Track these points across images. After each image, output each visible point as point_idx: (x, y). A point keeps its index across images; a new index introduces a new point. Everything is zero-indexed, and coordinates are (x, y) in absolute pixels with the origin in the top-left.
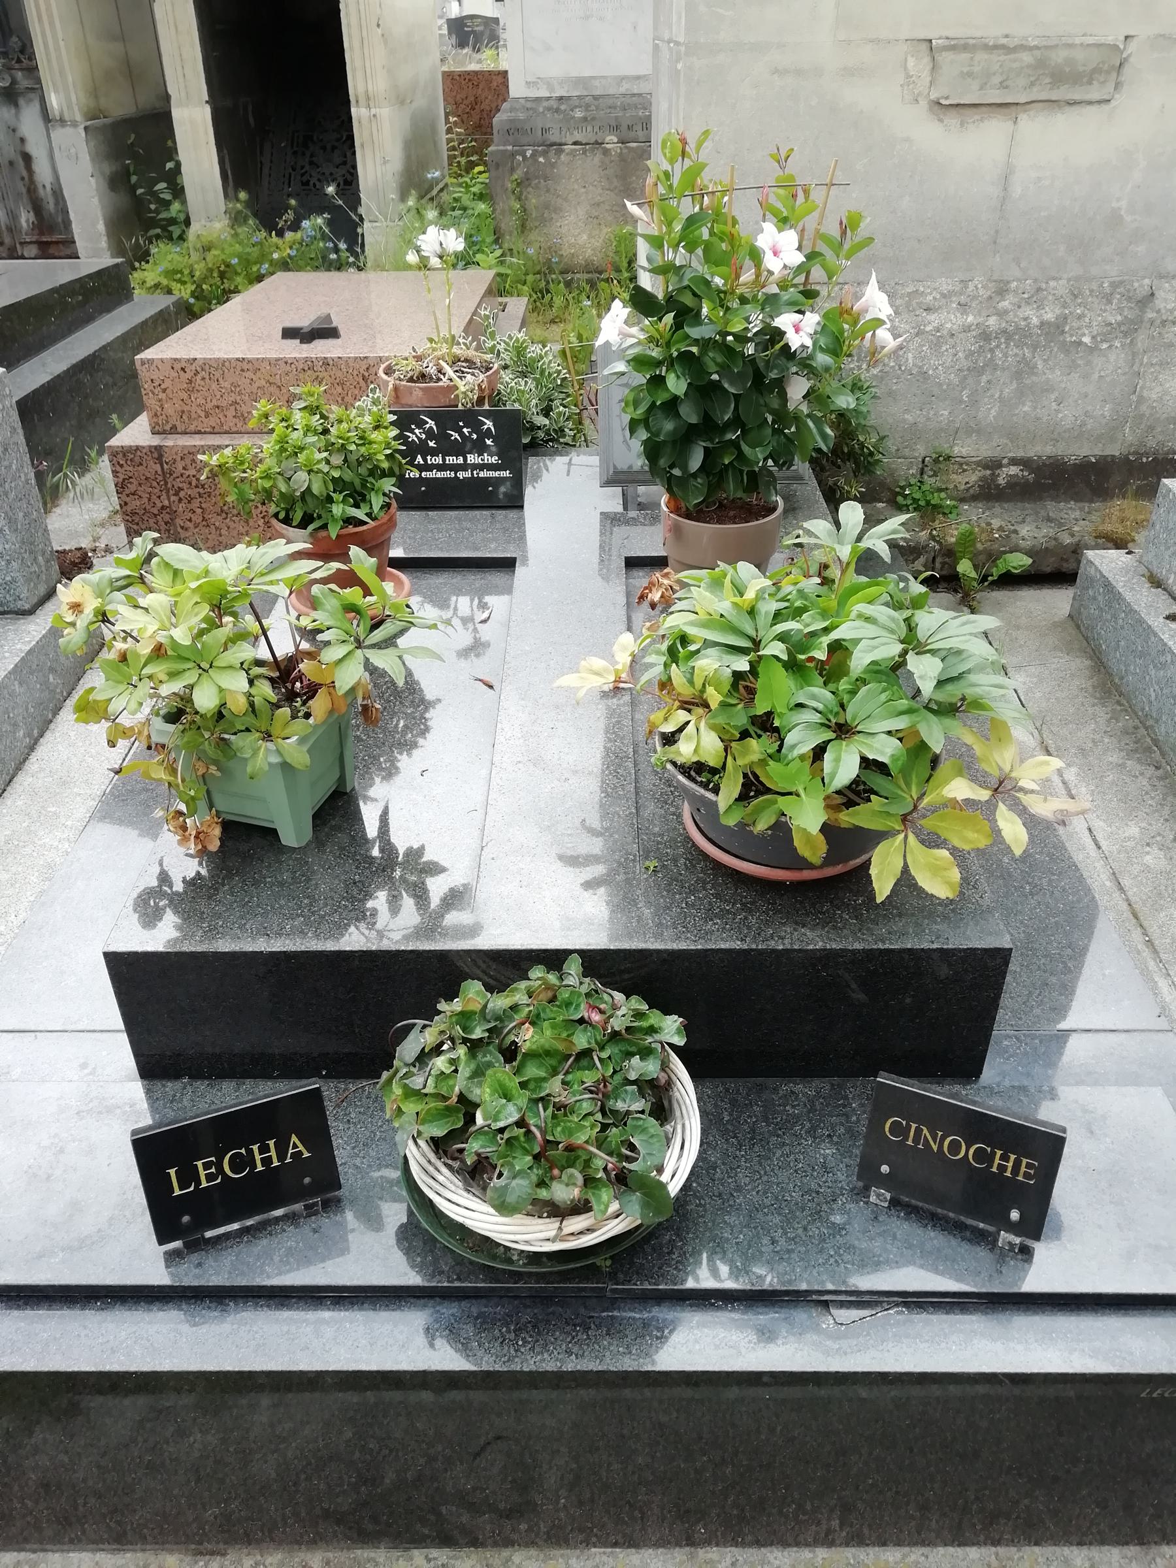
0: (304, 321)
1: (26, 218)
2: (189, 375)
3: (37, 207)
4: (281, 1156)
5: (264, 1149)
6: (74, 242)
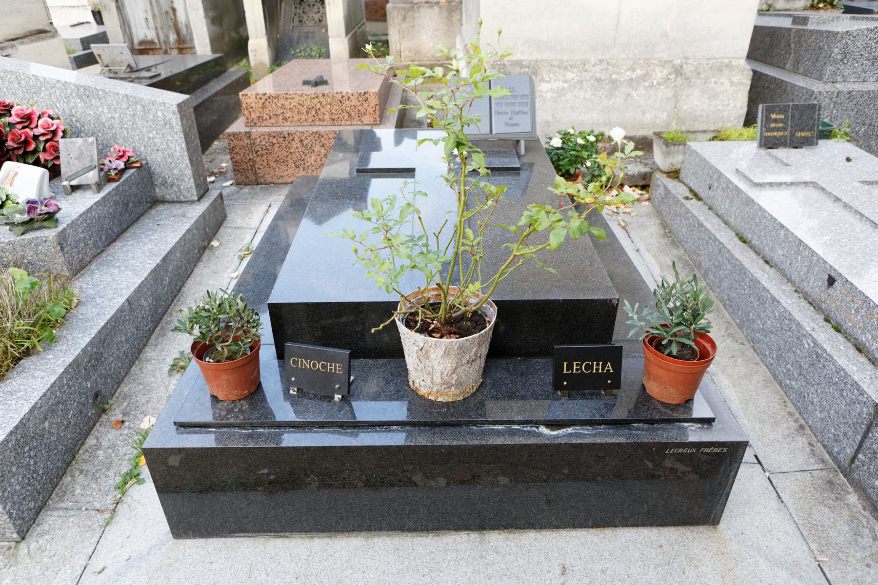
0: (312, 77)
1: (173, 37)
2: (263, 100)
3: (178, 32)
4: (603, 369)
5: (598, 365)
6: (194, 48)
